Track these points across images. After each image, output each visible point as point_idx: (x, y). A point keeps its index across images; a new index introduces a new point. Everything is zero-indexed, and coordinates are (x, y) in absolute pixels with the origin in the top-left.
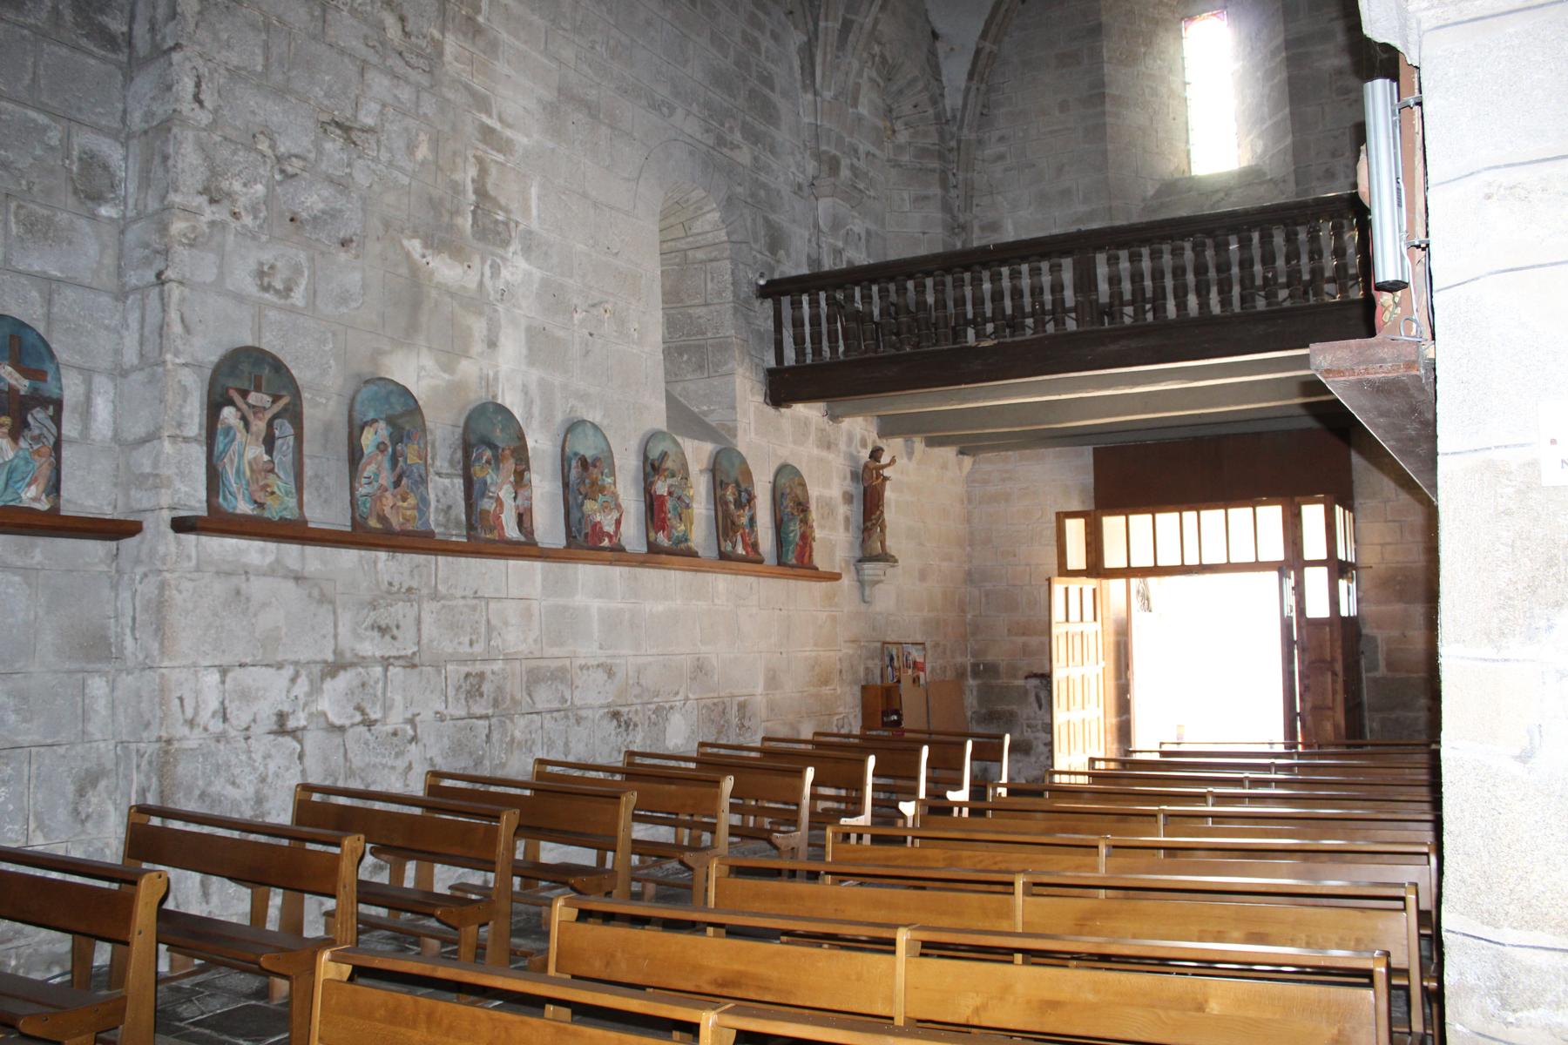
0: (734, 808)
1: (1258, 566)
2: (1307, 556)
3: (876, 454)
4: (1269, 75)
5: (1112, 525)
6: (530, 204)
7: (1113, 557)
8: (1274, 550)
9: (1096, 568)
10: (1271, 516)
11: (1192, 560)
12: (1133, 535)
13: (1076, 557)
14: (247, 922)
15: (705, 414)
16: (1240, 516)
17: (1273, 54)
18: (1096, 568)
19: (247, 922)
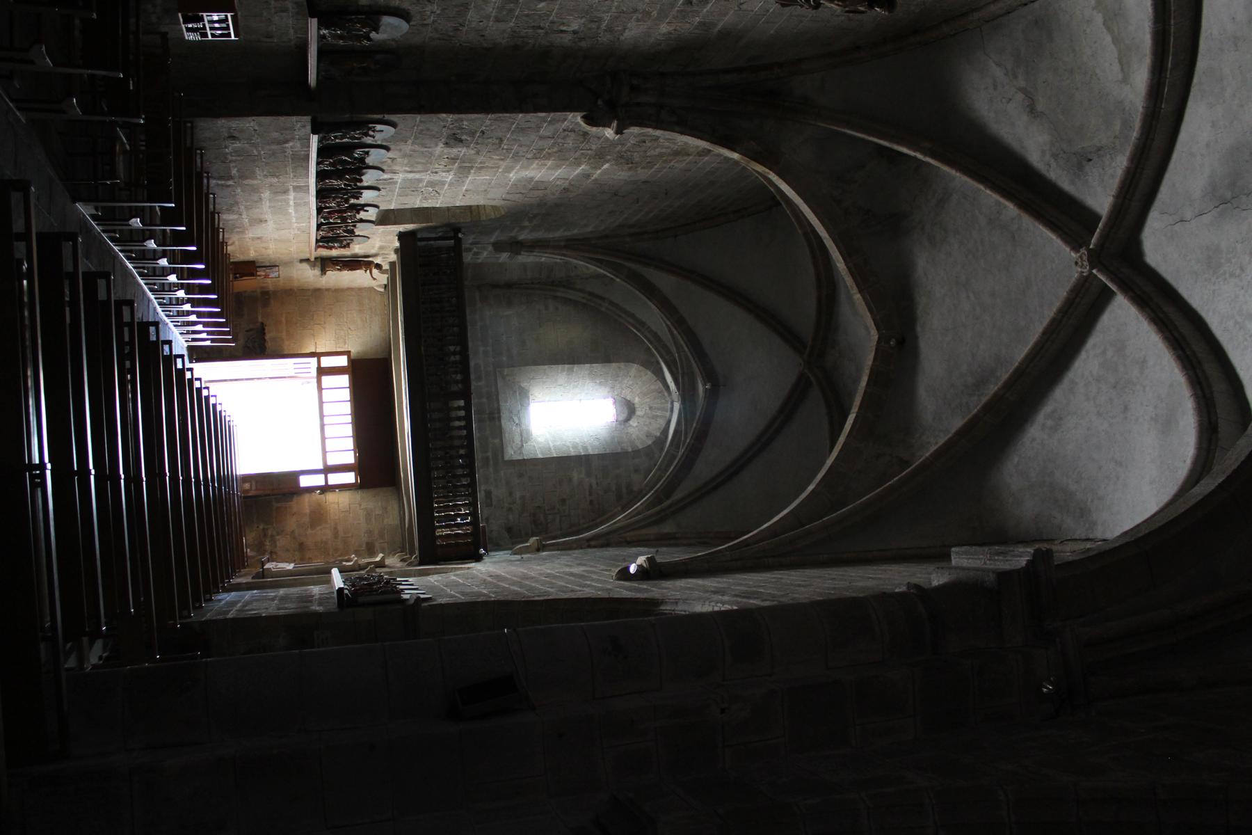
0: (396, 183)
1: (324, 452)
2: (330, 476)
3: (378, 266)
4: (575, 446)
5: (344, 380)
6: (269, 217)
7: (327, 380)
8: (332, 461)
9: (322, 372)
10: (350, 458)
11: (326, 420)
12: (339, 389)
13: (327, 362)
14: (507, 458)
15: (559, 167)
16: (350, 443)
17: (585, 448)
18: (322, 372)
19: (507, 458)
